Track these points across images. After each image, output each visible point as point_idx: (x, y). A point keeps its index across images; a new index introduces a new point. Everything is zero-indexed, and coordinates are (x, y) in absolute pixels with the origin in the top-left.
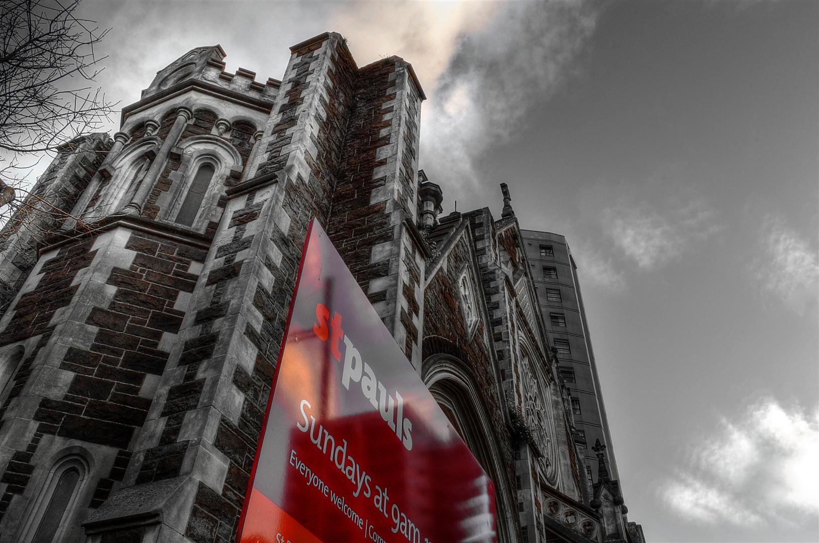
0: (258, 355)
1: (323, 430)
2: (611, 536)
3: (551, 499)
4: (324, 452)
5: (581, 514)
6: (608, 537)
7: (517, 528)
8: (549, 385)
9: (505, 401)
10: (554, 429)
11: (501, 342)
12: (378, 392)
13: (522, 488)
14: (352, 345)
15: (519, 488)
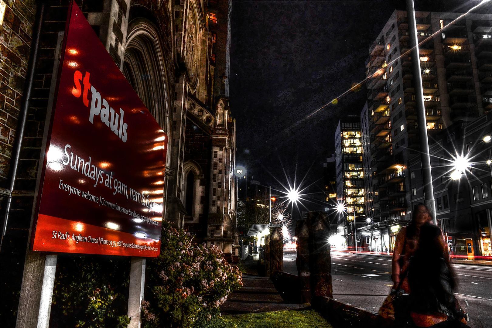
0: (6, 9)
1: (78, 158)
2: (220, 125)
3: (192, 101)
4: (77, 156)
5: (207, 112)
6: (218, 126)
7: (171, 122)
8: (202, 30)
9: (175, 48)
10: (200, 57)
11: (179, 5)
12: (110, 114)
13: (177, 100)
14: (96, 90)
15: (176, 99)
